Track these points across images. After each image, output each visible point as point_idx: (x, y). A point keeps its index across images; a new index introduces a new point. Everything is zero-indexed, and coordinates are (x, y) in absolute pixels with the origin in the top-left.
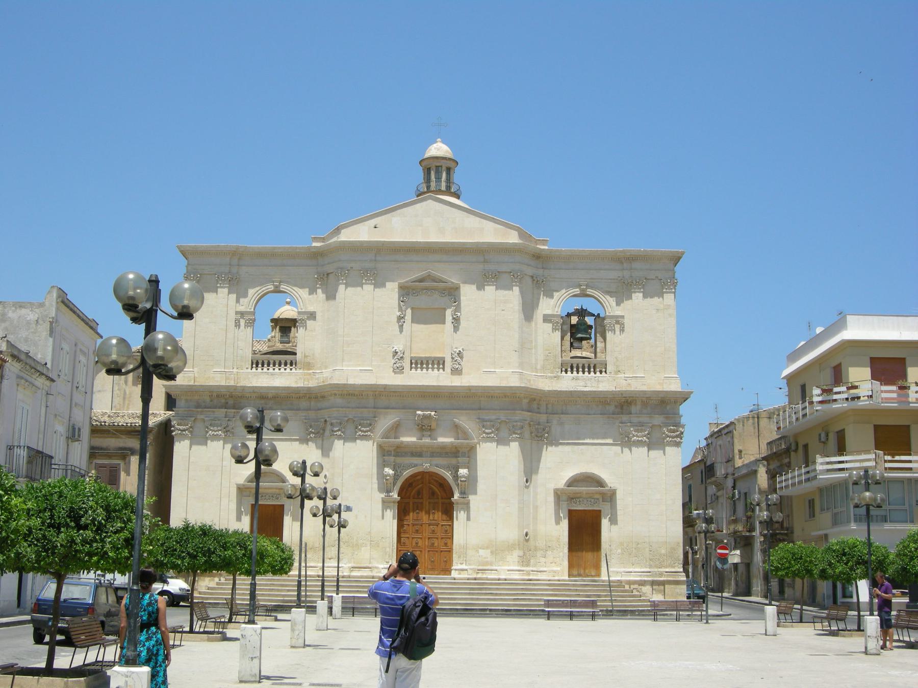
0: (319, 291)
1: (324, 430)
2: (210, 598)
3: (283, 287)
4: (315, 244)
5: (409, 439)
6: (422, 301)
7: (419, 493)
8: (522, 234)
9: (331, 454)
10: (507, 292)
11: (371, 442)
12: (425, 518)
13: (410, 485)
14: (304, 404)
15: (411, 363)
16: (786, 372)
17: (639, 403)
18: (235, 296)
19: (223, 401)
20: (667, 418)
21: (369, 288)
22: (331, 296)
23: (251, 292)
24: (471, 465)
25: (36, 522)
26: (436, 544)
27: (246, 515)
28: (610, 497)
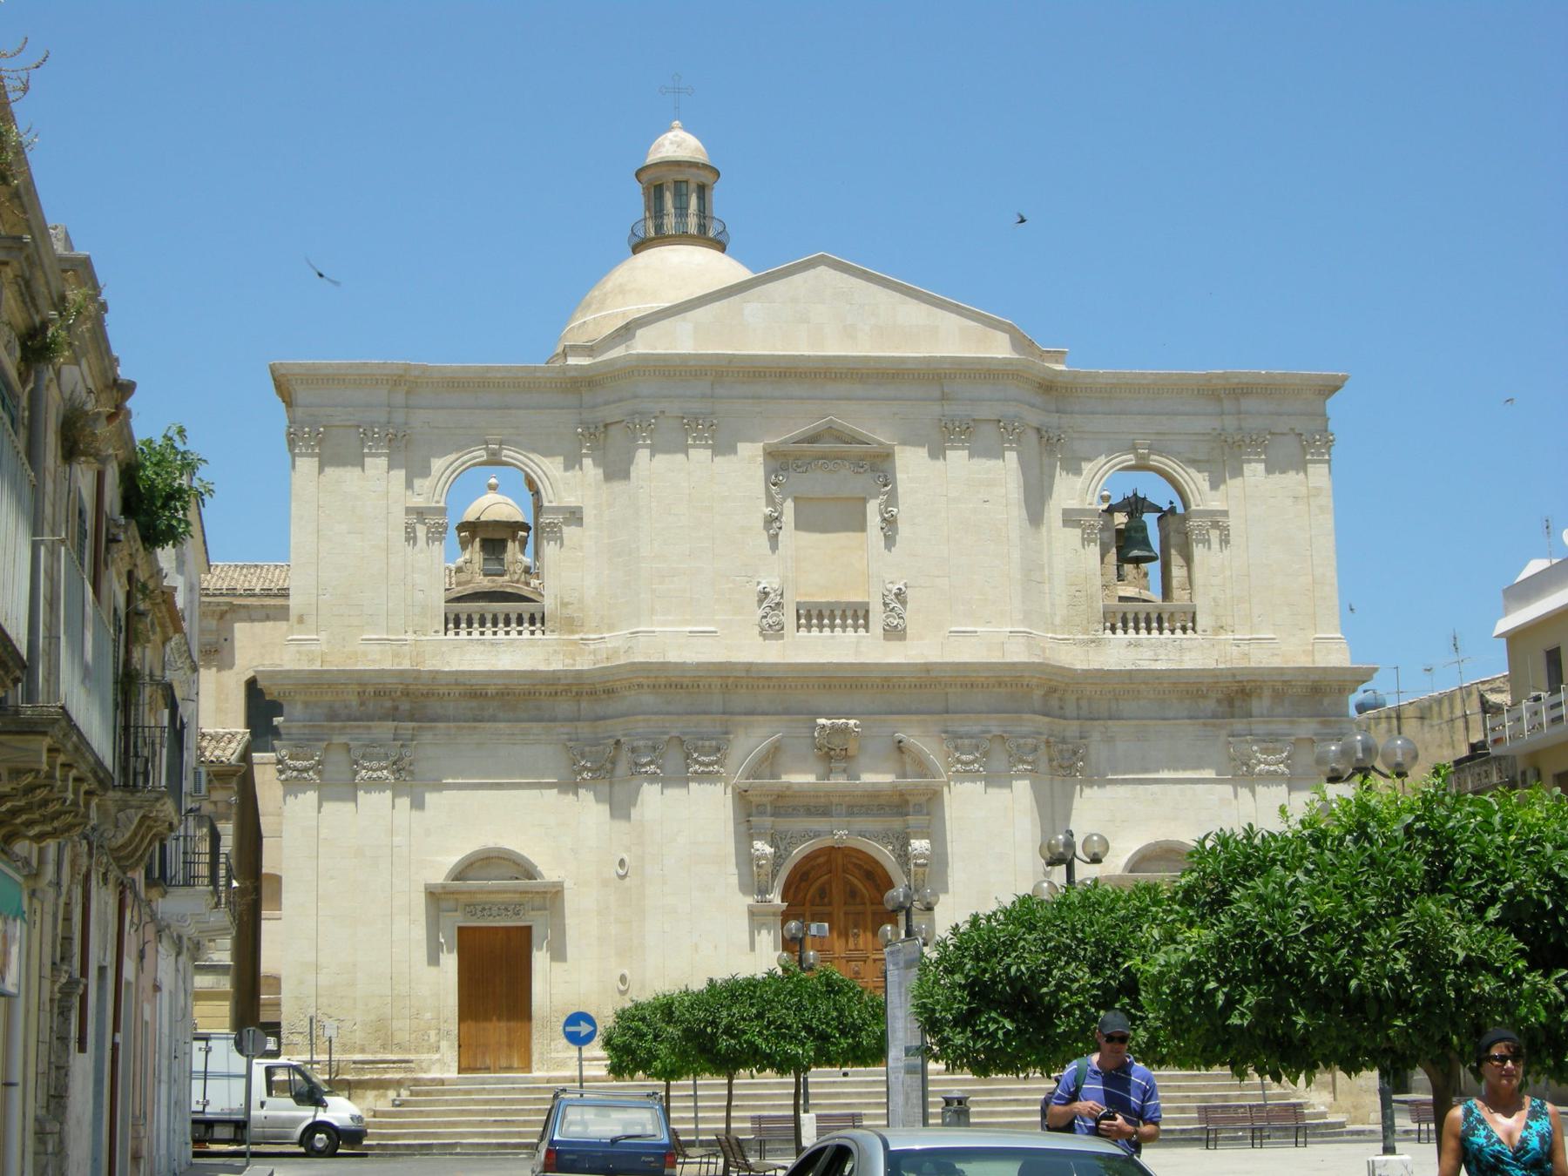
0: (587, 462)
1: (613, 763)
2: (404, 1136)
3: (508, 454)
4: (572, 361)
5: (802, 778)
6: (816, 482)
7: (823, 893)
8: (1020, 341)
9: (634, 812)
10: (991, 463)
11: (720, 787)
14: (565, 707)
15: (799, 617)
16: (1507, 623)
17: (1267, 693)
18: (401, 474)
19: (389, 704)
20: (1324, 723)
21: (700, 455)
22: (617, 471)
23: (438, 464)
25: (999, 969)
27: (450, 951)
28: (552, 897)
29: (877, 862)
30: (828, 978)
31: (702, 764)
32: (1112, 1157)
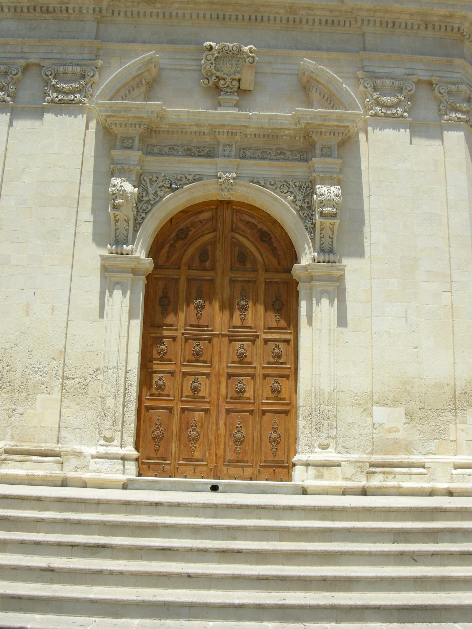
7: (204, 255)
11: (81, 120)
12: (218, 319)
13: (183, 234)
24: (348, 177)
26: (249, 393)
29: (274, 222)
30: (240, 48)
31: (59, 91)
32: (131, 293)
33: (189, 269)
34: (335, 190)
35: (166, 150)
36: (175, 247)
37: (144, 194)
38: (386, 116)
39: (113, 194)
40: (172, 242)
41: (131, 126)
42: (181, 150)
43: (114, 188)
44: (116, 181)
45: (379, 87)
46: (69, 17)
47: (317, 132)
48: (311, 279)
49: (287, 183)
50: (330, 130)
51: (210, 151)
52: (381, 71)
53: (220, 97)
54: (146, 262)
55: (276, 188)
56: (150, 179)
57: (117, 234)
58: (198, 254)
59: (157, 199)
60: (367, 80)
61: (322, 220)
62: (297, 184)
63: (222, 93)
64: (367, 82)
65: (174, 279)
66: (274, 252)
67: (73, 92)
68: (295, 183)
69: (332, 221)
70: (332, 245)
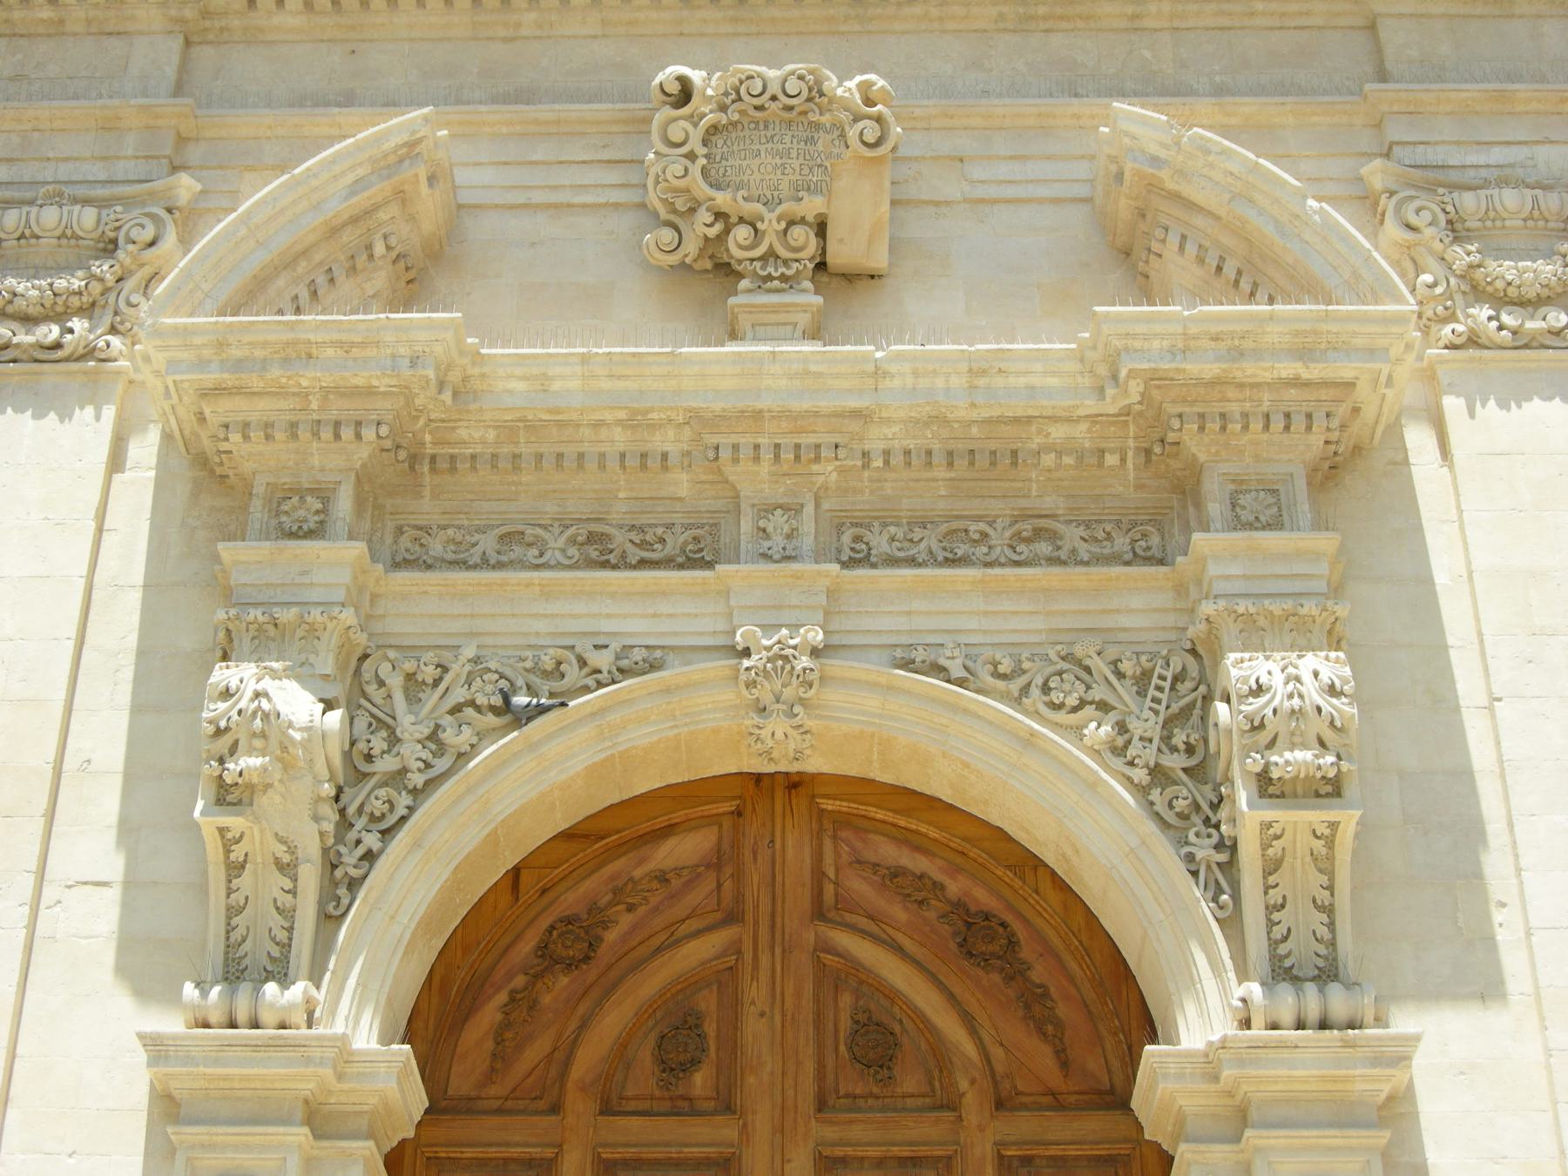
7: (682, 1040)
11: (90, 429)
13: (573, 946)
24: (1374, 597)
29: (1028, 864)
30: (819, 82)
33: (607, 1109)
34: (1319, 667)
35: (488, 543)
36: (533, 1005)
37: (378, 744)
38: (1524, 342)
39: (219, 733)
40: (519, 981)
41: (316, 435)
42: (556, 542)
43: (222, 706)
44: (240, 675)
45: (1472, 224)
46: (61, 22)
47: (1202, 416)
48: (1238, 1119)
49: (1079, 663)
50: (1265, 406)
51: (696, 539)
52: (1472, 159)
53: (732, 301)
54: (383, 1068)
55: (1025, 690)
56: (410, 677)
57: (236, 936)
58: (653, 1036)
59: (442, 765)
60: (1412, 198)
61: (1269, 815)
62: (1126, 667)
63: (744, 284)
64: (1416, 204)
65: (529, 1163)
66: (1034, 1005)
67: (59, 314)
68: (1115, 663)
69: (1316, 817)
70: (1333, 943)
